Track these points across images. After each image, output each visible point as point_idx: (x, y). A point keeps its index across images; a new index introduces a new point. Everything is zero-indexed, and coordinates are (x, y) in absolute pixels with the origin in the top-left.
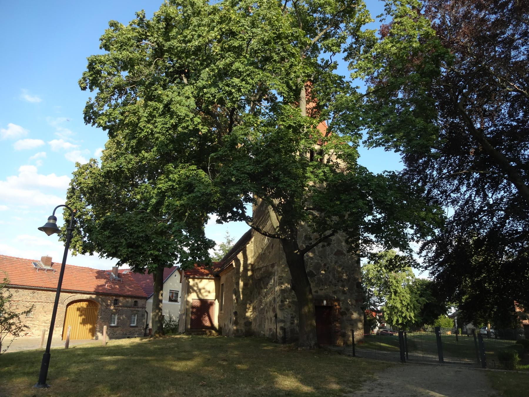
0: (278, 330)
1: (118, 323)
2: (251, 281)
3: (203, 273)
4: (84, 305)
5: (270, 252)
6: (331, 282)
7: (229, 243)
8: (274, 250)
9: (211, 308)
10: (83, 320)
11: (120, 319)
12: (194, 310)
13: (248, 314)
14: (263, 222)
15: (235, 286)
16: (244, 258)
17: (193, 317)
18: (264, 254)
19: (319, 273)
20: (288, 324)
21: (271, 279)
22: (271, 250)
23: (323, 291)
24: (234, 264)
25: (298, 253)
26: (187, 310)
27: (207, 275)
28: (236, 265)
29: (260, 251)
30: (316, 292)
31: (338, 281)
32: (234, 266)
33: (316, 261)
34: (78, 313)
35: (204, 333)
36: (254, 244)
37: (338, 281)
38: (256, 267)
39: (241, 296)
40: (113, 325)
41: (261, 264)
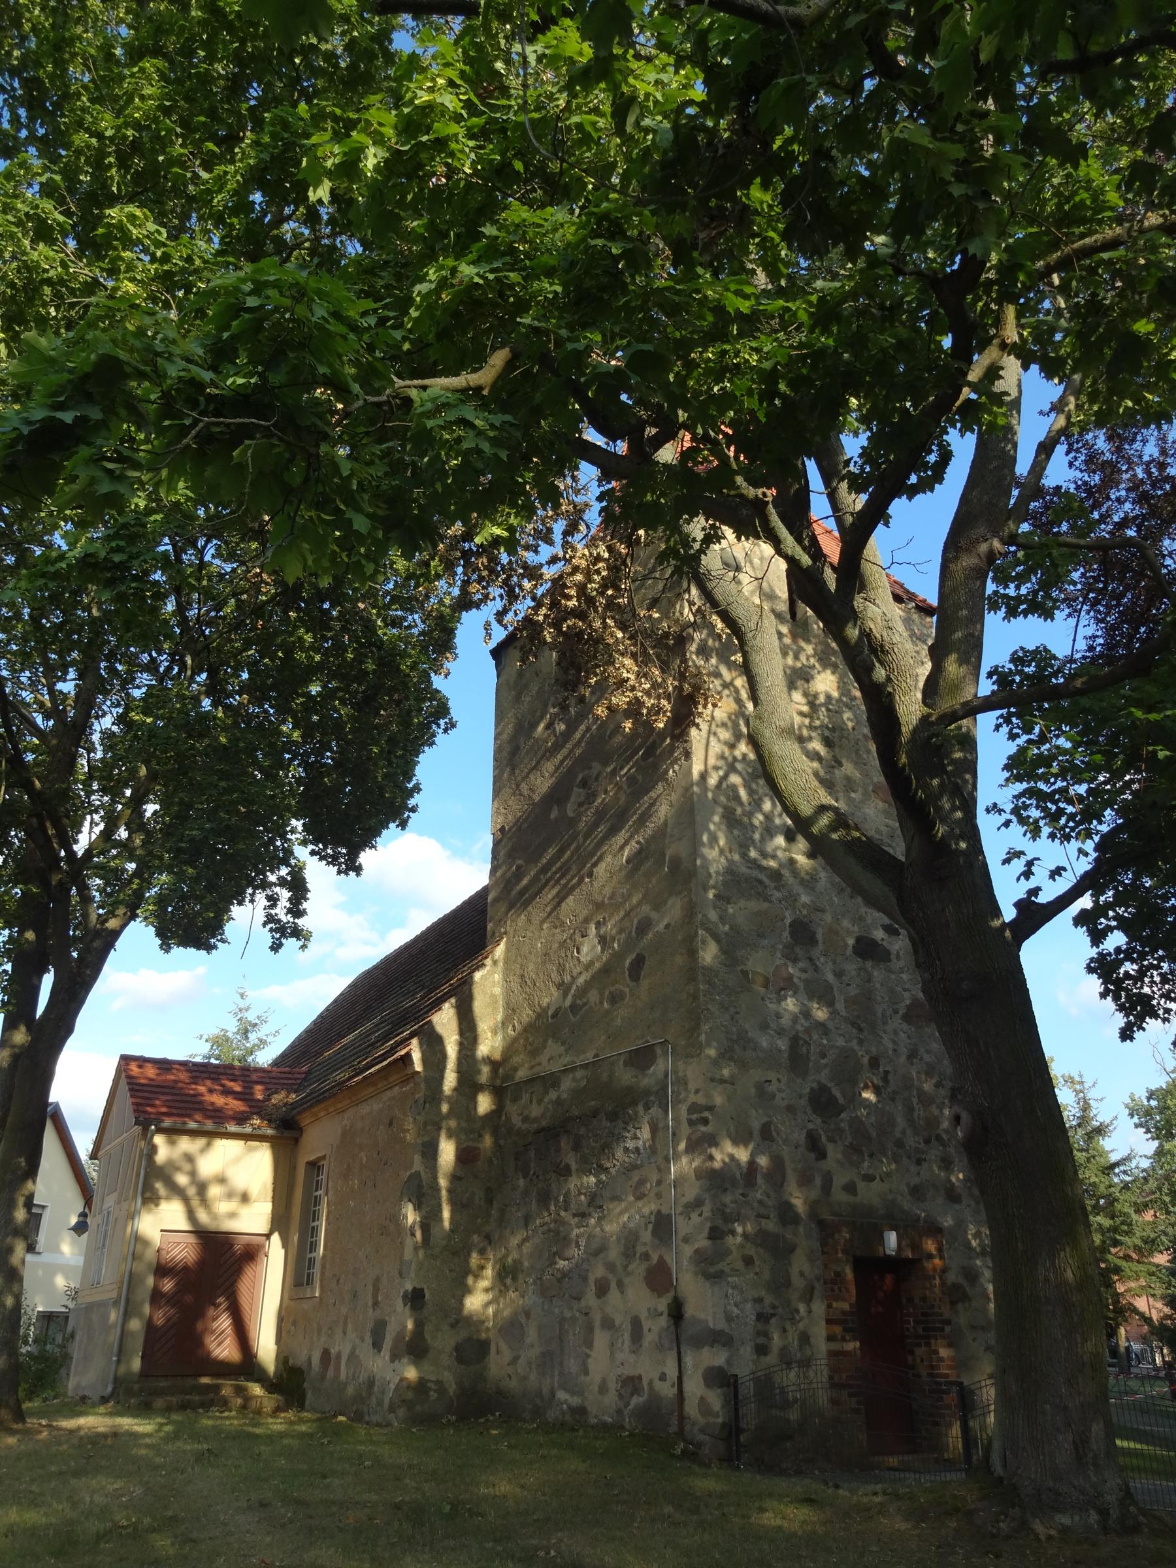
0: (694, 1387)
2: (488, 1141)
5: (615, 999)
6: (900, 1144)
7: (246, 1032)
8: (645, 983)
9: (249, 1272)
12: (168, 1285)
13: (475, 1302)
14: (564, 869)
15: (418, 1164)
16: (461, 1033)
17: (160, 1318)
18: (574, 1008)
21: (634, 1120)
22: (624, 985)
23: (876, 1185)
24: (416, 1056)
26: (133, 1281)
27: (241, 1119)
28: (425, 1061)
29: (549, 997)
30: (850, 1188)
32: (418, 1067)
33: (840, 1042)
35: (211, 1400)
36: (507, 972)
37: (927, 1141)
38: (522, 1074)
39: (446, 1214)
41: (553, 1057)
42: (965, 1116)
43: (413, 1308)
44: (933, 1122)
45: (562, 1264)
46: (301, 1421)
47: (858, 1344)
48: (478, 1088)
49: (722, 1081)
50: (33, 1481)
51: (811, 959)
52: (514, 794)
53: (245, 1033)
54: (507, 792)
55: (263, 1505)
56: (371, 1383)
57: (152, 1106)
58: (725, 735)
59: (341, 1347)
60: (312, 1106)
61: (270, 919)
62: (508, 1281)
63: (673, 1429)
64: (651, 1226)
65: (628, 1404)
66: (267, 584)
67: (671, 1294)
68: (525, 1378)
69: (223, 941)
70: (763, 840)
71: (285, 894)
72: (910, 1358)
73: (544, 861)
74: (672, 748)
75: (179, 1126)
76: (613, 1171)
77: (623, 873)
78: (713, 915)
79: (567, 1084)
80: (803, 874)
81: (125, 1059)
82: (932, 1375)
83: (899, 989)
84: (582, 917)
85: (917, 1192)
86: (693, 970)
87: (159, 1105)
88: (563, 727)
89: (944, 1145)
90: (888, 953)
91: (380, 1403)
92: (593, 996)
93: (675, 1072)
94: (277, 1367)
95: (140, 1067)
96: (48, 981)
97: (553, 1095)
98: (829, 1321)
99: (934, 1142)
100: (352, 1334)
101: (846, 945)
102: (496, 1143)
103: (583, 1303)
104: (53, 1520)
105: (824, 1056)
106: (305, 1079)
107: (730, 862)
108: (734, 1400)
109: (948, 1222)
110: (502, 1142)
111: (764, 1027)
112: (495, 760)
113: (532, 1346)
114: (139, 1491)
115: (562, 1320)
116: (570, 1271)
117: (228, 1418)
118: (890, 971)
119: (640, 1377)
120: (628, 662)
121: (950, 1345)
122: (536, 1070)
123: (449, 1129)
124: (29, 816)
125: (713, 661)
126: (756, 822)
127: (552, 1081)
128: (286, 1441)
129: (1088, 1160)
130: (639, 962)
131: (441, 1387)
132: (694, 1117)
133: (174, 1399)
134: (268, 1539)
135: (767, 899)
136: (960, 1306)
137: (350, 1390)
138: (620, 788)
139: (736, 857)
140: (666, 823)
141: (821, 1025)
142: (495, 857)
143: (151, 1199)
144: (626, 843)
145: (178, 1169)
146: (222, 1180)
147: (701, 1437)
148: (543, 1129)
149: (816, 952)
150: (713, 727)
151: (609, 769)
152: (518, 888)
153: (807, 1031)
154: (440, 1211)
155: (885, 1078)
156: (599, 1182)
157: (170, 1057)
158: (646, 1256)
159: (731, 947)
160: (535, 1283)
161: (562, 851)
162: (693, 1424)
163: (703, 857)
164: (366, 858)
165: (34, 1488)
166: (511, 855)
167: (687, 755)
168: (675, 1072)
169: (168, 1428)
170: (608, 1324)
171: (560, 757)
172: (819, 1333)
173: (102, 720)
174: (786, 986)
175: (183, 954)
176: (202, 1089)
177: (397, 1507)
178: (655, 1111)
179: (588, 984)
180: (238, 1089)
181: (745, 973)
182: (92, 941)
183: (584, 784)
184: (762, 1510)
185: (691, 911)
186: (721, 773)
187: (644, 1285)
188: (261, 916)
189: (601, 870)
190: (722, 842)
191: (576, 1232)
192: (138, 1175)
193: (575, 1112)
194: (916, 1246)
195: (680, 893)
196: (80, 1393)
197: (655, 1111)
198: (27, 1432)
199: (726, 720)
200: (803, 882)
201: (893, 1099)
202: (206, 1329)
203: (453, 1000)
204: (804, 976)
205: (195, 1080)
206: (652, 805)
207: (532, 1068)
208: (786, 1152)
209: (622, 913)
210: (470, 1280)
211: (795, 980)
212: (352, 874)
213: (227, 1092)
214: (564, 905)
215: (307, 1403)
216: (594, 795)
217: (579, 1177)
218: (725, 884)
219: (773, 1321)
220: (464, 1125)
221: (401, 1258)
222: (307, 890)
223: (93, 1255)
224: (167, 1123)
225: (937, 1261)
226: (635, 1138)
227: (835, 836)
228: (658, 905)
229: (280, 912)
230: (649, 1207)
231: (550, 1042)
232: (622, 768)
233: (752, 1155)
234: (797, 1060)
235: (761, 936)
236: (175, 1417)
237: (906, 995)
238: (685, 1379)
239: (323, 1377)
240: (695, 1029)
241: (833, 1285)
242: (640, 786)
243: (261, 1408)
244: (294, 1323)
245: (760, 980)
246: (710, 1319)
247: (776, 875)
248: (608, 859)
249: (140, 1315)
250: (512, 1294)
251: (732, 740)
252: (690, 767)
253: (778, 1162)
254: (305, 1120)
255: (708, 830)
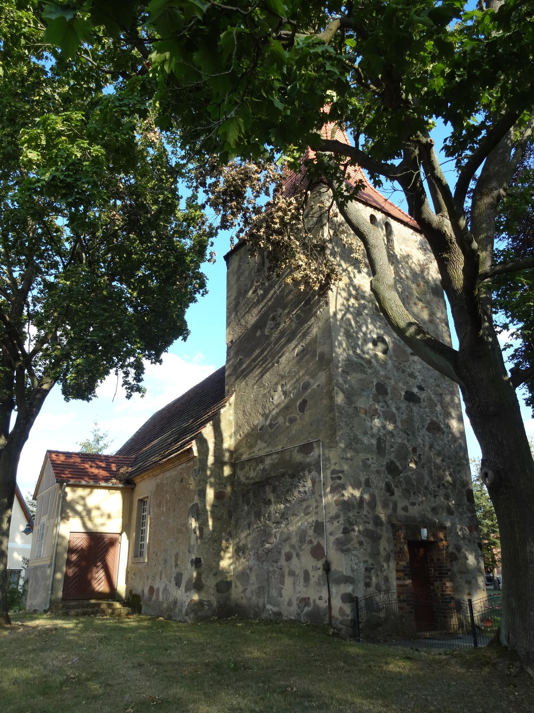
0: (336, 603)
2: (229, 489)
3: (96, 476)
6: (426, 488)
8: (307, 413)
9: (112, 551)
12: (74, 557)
13: (225, 563)
14: (265, 360)
15: (196, 500)
16: (215, 438)
17: (71, 572)
18: (271, 425)
19: (406, 467)
21: (303, 477)
22: (297, 414)
23: (416, 507)
24: (195, 449)
26: (57, 555)
27: (107, 480)
28: (199, 451)
29: (258, 420)
30: (405, 509)
32: (196, 454)
33: (399, 441)
35: (97, 611)
37: (439, 487)
38: (245, 457)
39: (210, 523)
42: (490, 473)
43: (196, 567)
44: (441, 478)
45: (267, 545)
46: (142, 620)
47: (411, 581)
48: (224, 464)
49: (347, 459)
50: (21, 654)
51: (385, 402)
52: (237, 325)
53: (98, 441)
54: (233, 324)
55: (140, 665)
56: (175, 602)
57: (64, 474)
58: (344, 294)
59: (159, 585)
60: (141, 473)
61: (126, 383)
62: (241, 554)
63: (326, 622)
64: (313, 528)
65: (303, 611)
66: (119, 220)
67: (324, 559)
68: (250, 599)
69: (95, 396)
70: (362, 344)
71: (132, 371)
72: (432, 587)
73: (254, 356)
74: (319, 301)
75: (77, 483)
76: (293, 502)
77: (295, 361)
78: (341, 380)
79: (268, 461)
80: (381, 361)
81: (49, 452)
82: (442, 595)
83: (425, 416)
84: (274, 382)
85: (434, 510)
86: (332, 407)
87: (67, 473)
88: (262, 292)
89: (446, 489)
90: (420, 399)
91: (180, 611)
92: (281, 420)
93: (324, 455)
94: (126, 595)
95: (57, 456)
96: (14, 415)
97: (261, 467)
98: (397, 571)
99: (441, 487)
100: (164, 579)
101: (401, 395)
102: (233, 490)
103: (279, 564)
104: (36, 675)
105: (392, 447)
106: (135, 461)
107: (348, 355)
108: (356, 609)
109: (448, 524)
110: (236, 489)
111: (365, 433)
112: (227, 308)
113: (253, 584)
114: (76, 659)
115: (268, 572)
116: (272, 549)
117: (106, 619)
118: (421, 407)
119: (309, 598)
120: (302, 256)
121: (451, 581)
122: (252, 454)
123: (211, 483)
124: (5, 333)
125: (338, 259)
126: (359, 336)
127: (260, 460)
128: (140, 631)
129: (482, 495)
130: (304, 403)
131: (210, 605)
132: (334, 476)
133: (79, 611)
134: (148, 684)
135: (365, 373)
136: (454, 563)
137: (165, 605)
138: (292, 321)
139: (351, 352)
140: (316, 336)
141: (391, 432)
142: (228, 355)
143: (65, 517)
144: (296, 346)
145: (78, 503)
146: (98, 508)
147: (340, 626)
148: (257, 483)
149: (388, 398)
150: (339, 290)
151: (286, 311)
152: (241, 369)
153: (384, 435)
154: (207, 521)
155: (419, 458)
156: (286, 507)
157: (71, 451)
158: (311, 542)
159: (349, 397)
160: (254, 554)
161: (263, 351)
162: (337, 620)
163: (336, 353)
164: (164, 356)
165: (22, 658)
166: (237, 354)
167: (327, 303)
168: (324, 455)
169: (81, 625)
170: (292, 573)
171: (261, 306)
172: (393, 575)
173: (33, 291)
174: (374, 414)
175: (77, 403)
176: (87, 466)
177: (207, 665)
178: (314, 473)
179: (278, 414)
180: (104, 465)
181: (356, 408)
182: (36, 395)
183: (274, 319)
184: (387, 663)
185: (330, 379)
186: (343, 312)
187: (310, 555)
188: (121, 382)
189: (283, 360)
190: (344, 346)
191: (274, 530)
192: (58, 506)
193: (273, 474)
194: (435, 535)
195: (325, 369)
196: (33, 609)
197: (314, 473)
198: (13, 629)
199: (344, 287)
200: (381, 365)
201: (423, 467)
202: (92, 578)
203: (211, 422)
204: (382, 409)
205: (83, 462)
206: (309, 328)
207: (250, 454)
208: (376, 492)
209: (295, 380)
210: (222, 553)
211: (379, 411)
212: (158, 364)
213: (99, 467)
214: (264, 377)
215: (143, 611)
216: (279, 324)
217: (276, 505)
218: (346, 365)
219: (372, 571)
220: (217, 481)
221: (189, 544)
222: (144, 369)
223: (37, 545)
224: (72, 481)
225: (444, 542)
226: (304, 486)
227: (418, 337)
228: (313, 376)
229: (130, 379)
230: (312, 519)
231: (259, 441)
232: (293, 311)
233: (361, 493)
234: (380, 449)
235: (363, 390)
236: (81, 619)
237: (428, 418)
238: (332, 599)
239: (150, 599)
240: (334, 434)
241: (399, 553)
242: (302, 320)
243: (120, 614)
244: (134, 574)
245: (363, 411)
246: (344, 570)
247: (369, 362)
248: (287, 354)
249: (61, 571)
250: (242, 560)
251: (347, 297)
252: (329, 310)
253: (373, 497)
254: (137, 480)
255: (338, 340)
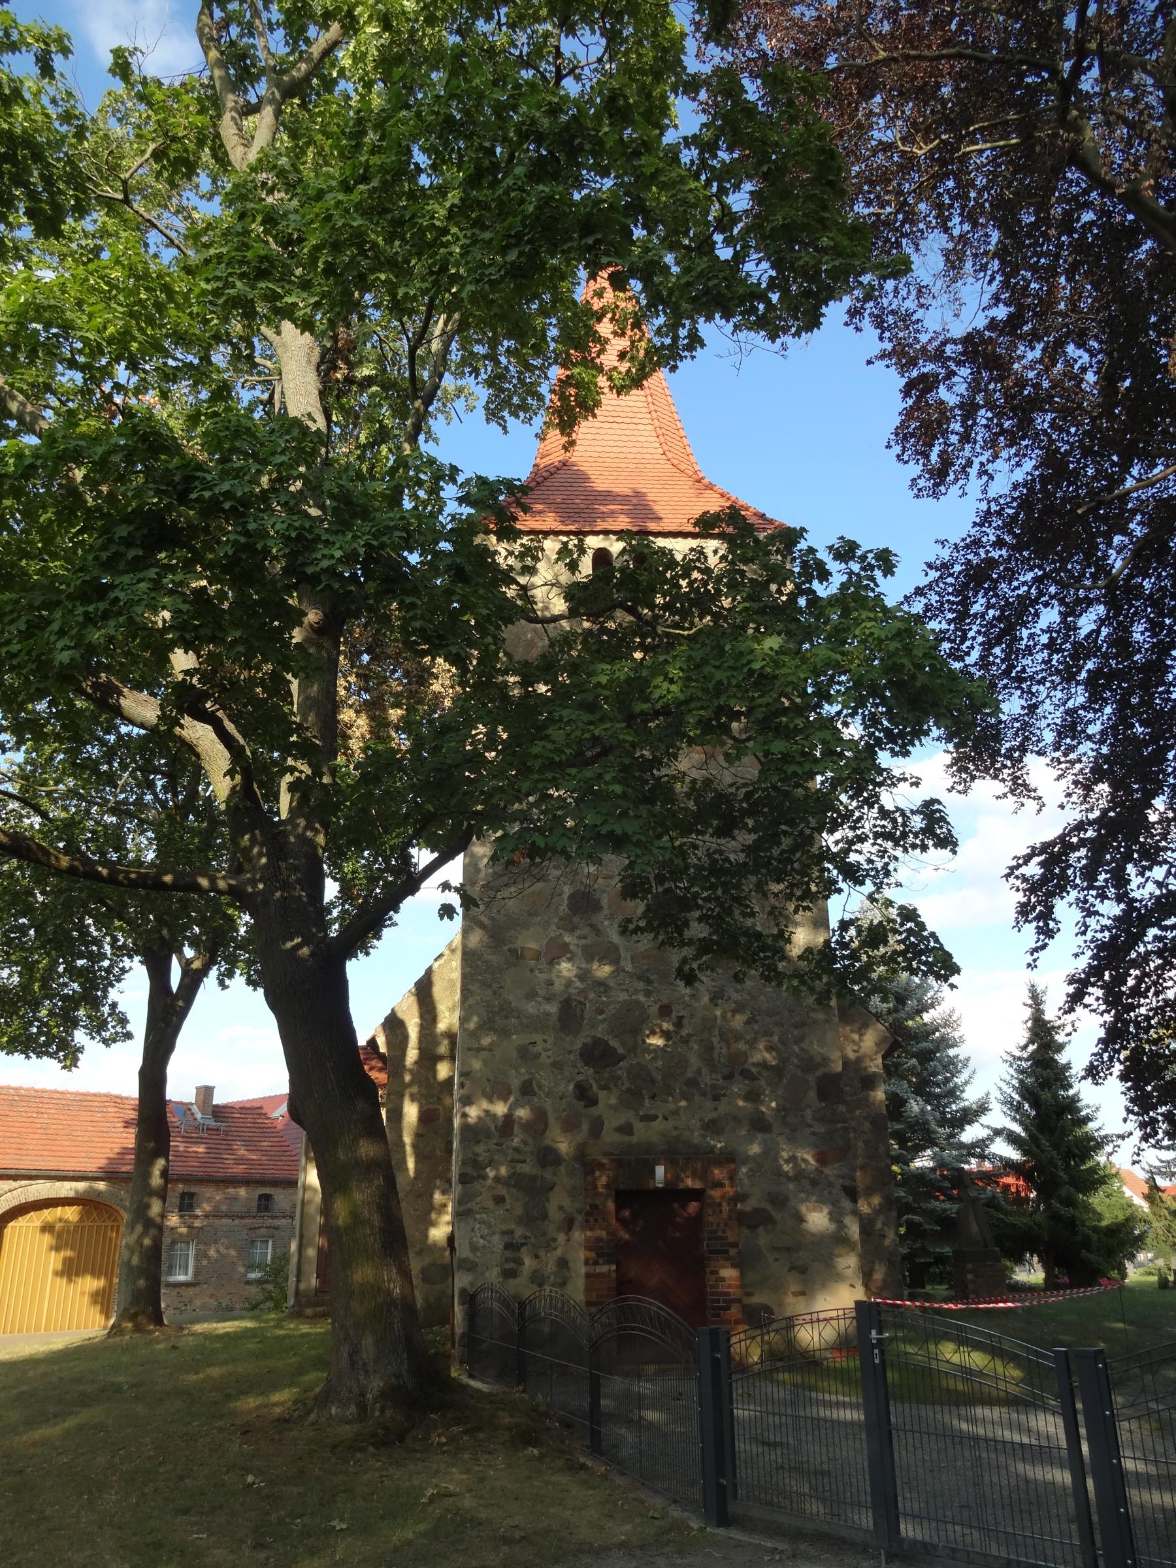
1: (197, 1273)
4: (71, 1214)
6: (693, 1083)
10: (67, 1263)
11: (206, 1256)
16: (422, 1017)
19: (638, 1047)
20: (493, 1275)
23: (658, 1125)
25: (305, 951)
28: (389, 1043)
31: (729, 1077)
33: (623, 996)
34: (47, 1239)
39: (411, 1164)
40: (182, 1278)
49: (480, 1049)
105: (601, 1012)
111: (531, 995)
155: (679, 1023)
172: (579, 1258)
208: (548, 1104)
210: (433, 1216)
219: (524, 1249)
241: (593, 1215)
